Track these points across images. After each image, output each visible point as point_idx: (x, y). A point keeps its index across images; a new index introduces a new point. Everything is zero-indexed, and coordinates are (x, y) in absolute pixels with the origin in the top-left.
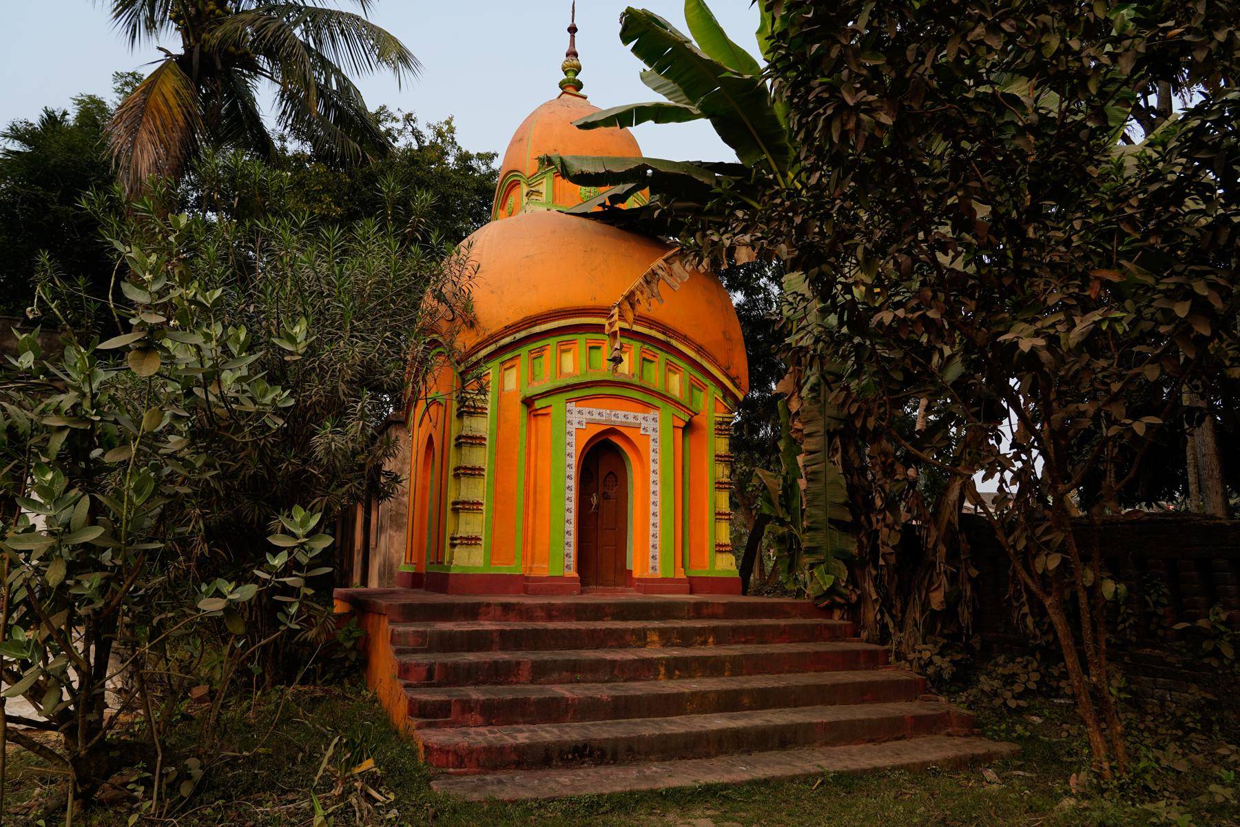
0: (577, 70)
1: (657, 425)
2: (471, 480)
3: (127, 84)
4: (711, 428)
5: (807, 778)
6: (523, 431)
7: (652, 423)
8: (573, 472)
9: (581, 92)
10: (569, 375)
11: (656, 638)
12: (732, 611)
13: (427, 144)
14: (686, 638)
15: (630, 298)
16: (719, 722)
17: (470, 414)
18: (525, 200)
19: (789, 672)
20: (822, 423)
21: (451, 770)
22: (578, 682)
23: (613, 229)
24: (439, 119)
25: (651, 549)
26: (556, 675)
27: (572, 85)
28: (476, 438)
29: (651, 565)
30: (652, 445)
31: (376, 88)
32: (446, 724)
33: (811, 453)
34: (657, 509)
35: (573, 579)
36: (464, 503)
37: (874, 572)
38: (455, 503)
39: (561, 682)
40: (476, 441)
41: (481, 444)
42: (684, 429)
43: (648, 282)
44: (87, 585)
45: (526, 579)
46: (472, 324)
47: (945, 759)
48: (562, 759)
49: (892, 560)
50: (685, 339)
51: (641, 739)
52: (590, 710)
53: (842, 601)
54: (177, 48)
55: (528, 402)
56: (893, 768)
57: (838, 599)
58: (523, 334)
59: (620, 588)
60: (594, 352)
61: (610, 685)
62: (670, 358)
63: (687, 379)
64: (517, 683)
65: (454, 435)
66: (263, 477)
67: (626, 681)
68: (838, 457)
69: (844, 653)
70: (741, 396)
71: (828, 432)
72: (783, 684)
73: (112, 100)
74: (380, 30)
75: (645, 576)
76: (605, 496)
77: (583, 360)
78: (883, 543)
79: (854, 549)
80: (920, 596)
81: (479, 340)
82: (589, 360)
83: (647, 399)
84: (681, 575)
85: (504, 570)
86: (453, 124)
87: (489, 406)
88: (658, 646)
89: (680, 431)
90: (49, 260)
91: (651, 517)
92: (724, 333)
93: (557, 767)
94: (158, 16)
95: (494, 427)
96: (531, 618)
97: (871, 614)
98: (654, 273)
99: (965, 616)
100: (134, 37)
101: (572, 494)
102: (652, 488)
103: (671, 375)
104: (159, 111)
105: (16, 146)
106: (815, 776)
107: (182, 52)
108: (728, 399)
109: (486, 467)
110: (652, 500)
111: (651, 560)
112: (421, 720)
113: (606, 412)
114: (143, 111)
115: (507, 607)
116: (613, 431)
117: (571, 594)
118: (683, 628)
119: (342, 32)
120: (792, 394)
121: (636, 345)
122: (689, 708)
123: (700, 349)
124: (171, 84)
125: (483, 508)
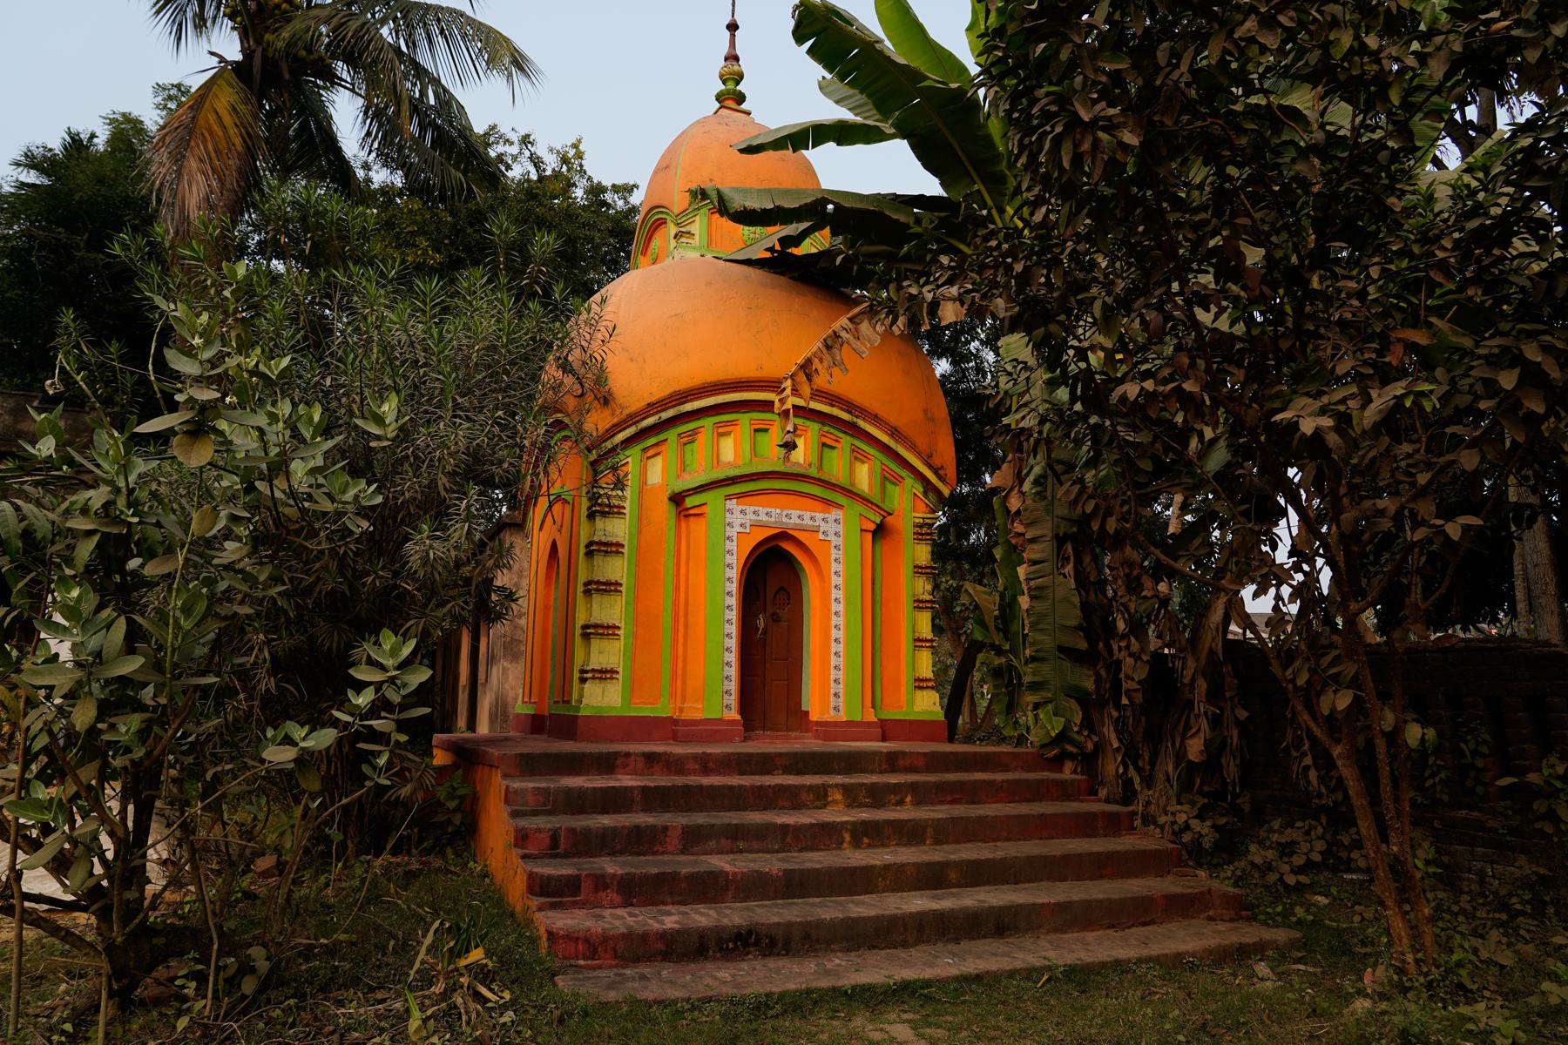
0: (739, 78)
1: (840, 528)
2: (606, 598)
3: (170, 98)
4: (908, 530)
5: (1030, 974)
8: (733, 587)
9: (744, 106)
11: (839, 797)
12: (935, 762)
14: (878, 795)
15: (806, 367)
16: (919, 903)
17: (604, 514)
18: (673, 243)
20: (1049, 524)
21: (581, 962)
22: (741, 852)
23: (782, 280)
24: (563, 141)
25: (833, 685)
26: (712, 844)
27: (732, 98)
28: (612, 544)
29: (832, 705)
30: (834, 554)
31: (484, 102)
32: (575, 905)
33: (1035, 563)
34: (840, 634)
35: (733, 722)
36: (596, 626)
37: (1115, 714)
38: (585, 627)
39: (720, 852)
40: (611, 548)
41: (618, 552)
42: (874, 533)
43: (828, 348)
44: (123, 729)
46: (606, 400)
47: (1205, 950)
48: (721, 949)
50: (875, 419)
51: (820, 923)
53: (1074, 750)
55: (677, 499)
56: (1139, 961)
57: (1070, 748)
58: (670, 413)
59: (793, 734)
60: (760, 436)
64: (663, 853)
65: (583, 541)
67: (800, 851)
69: (1077, 816)
70: (946, 492)
71: (1057, 536)
72: (999, 854)
73: (152, 119)
75: (826, 718)
76: (775, 618)
77: (746, 447)
79: (1089, 685)
81: (615, 420)
84: (871, 718)
85: (647, 711)
86: (582, 148)
87: (627, 504)
88: (841, 807)
89: (870, 536)
90: (74, 320)
91: (833, 644)
92: (925, 411)
93: (715, 959)
95: (635, 531)
96: (681, 772)
97: (1111, 767)
98: (836, 335)
99: (1231, 768)
100: (179, 39)
101: (733, 615)
102: (834, 607)
103: (858, 464)
104: (211, 132)
105: (31, 177)
106: (1041, 970)
108: (931, 495)
109: (624, 581)
110: (833, 623)
111: (832, 699)
112: (542, 900)
113: (775, 511)
114: (191, 132)
115: (651, 758)
116: (784, 535)
117: (732, 741)
118: (873, 784)
119: (442, 32)
120: (1012, 489)
121: (814, 427)
122: (881, 884)
123: (894, 432)
124: (225, 99)
125: (621, 632)
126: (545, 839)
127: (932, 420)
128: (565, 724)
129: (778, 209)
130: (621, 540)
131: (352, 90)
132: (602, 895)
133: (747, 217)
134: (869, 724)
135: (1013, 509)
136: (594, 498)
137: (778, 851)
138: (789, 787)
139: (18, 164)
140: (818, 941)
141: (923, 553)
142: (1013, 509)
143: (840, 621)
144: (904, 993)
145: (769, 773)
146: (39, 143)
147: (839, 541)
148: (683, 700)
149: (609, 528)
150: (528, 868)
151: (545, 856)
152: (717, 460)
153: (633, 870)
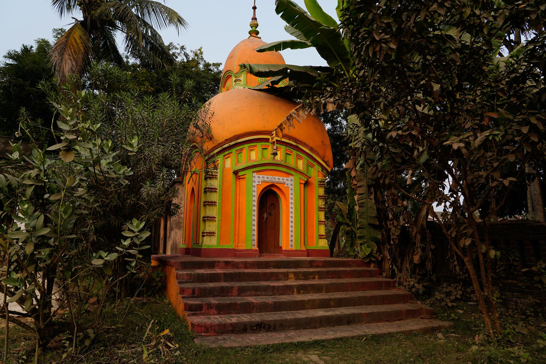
0: (257, 26)
1: (292, 183)
2: (211, 207)
3: (58, 34)
4: (316, 183)
5: (359, 337)
6: (234, 185)
7: (290, 181)
9: (259, 36)
10: (254, 161)
11: (292, 276)
12: (326, 264)
14: (306, 276)
15: (280, 127)
16: (320, 313)
17: (210, 178)
18: (234, 83)
19: (351, 291)
20: (365, 181)
21: (203, 334)
22: (258, 295)
24: (196, 48)
25: (290, 237)
26: (249, 293)
27: (254, 33)
28: (213, 189)
29: (290, 244)
30: (290, 192)
31: (168, 35)
32: (201, 314)
33: (360, 194)
34: (293, 220)
36: (208, 217)
37: (389, 247)
38: (204, 217)
39: (251, 295)
40: (213, 190)
41: (215, 191)
42: (304, 184)
43: (288, 120)
44: (43, 254)
45: (236, 250)
46: (211, 138)
48: (252, 329)
50: (305, 145)
51: (286, 320)
52: (264, 308)
53: (374, 260)
55: (236, 173)
56: (397, 333)
57: (373, 259)
58: (233, 143)
60: (264, 151)
62: (298, 153)
63: (306, 162)
64: (231, 296)
65: (203, 188)
66: (120, 206)
67: (279, 295)
68: (372, 197)
70: (329, 170)
71: (368, 185)
72: (348, 296)
73: (52, 41)
74: (170, 9)
75: (288, 249)
76: (270, 214)
77: (260, 154)
78: (393, 234)
79: (380, 237)
80: (409, 257)
81: (214, 145)
82: (262, 154)
83: (288, 171)
84: (303, 248)
85: (226, 247)
88: (293, 280)
89: (303, 185)
90: (25, 111)
92: (322, 142)
93: (250, 333)
95: (221, 184)
96: (237, 268)
97: (387, 265)
98: (291, 115)
100: (62, 13)
101: (255, 213)
102: (291, 210)
103: (299, 160)
104: (73, 46)
105: (10, 61)
106: (363, 336)
107: (82, 19)
109: (217, 201)
113: (270, 177)
114: (66, 45)
115: (227, 263)
116: (273, 185)
117: (255, 257)
120: (352, 169)
121: (283, 148)
122: (307, 307)
123: (311, 149)
124: (78, 34)
125: (216, 219)
127: (324, 145)
130: (216, 187)
132: (210, 310)
133: (260, 74)
136: (207, 173)
137: (271, 295)
138: (275, 273)
139: (6, 57)
140: (285, 327)
141: (322, 191)
144: (316, 344)
147: (292, 187)
148: (238, 243)
149: (212, 183)
150: (185, 301)
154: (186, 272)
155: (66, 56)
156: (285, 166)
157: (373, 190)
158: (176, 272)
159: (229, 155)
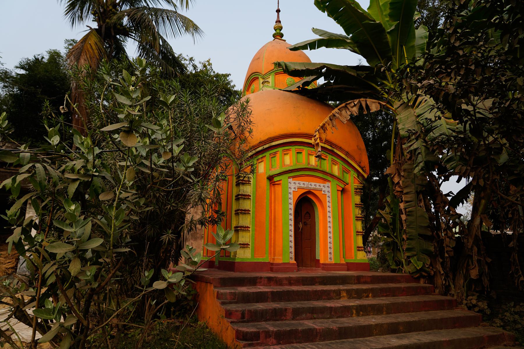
0: (281, 28)
1: (329, 189)
2: (244, 216)
3: (71, 45)
4: (352, 191)
6: (268, 192)
8: (292, 212)
9: (283, 38)
10: (288, 165)
11: (345, 294)
13: (199, 70)
15: (323, 127)
18: (261, 85)
20: (413, 187)
22: (315, 319)
23: (305, 98)
24: (204, 60)
25: (329, 249)
26: (304, 315)
27: (278, 35)
28: (246, 195)
29: (329, 257)
31: (180, 44)
32: (258, 344)
33: (407, 202)
35: (293, 264)
36: (241, 227)
37: (441, 260)
40: (246, 197)
41: (248, 199)
43: (331, 120)
44: (89, 274)
49: (452, 254)
50: (340, 149)
53: (426, 274)
54: (95, 25)
55: (270, 178)
57: (424, 274)
59: (314, 268)
60: (299, 155)
61: (331, 320)
62: (334, 158)
64: (286, 320)
67: (337, 318)
68: (422, 204)
70: (366, 176)
71: (417, 192)
72: (416, 319)
73: (63, 52)
74: (185, 18)
75: (327, 262)
78: (447, 246)
80: (463, 272)
82: (297, 158)
84: (343, 262)
85: (261, 260)
86: (210, 62)
88: (346, 298)
89: (340, 192)
90: (49, 104)
91: (329, 234)
92: (357, 146)
94: (84, 15)
95: (255, 190)
96: (281, 285)
97: (440, 281)
98: (334, 116)
99: (486, 282)
100: (73, 23)
101: (292, 223)
102: (328, 219)
103: (334, 166)
105: (22, 72)
107: (97, 27)
108: (360, 178)
109: (251, 210)
110: (328, 226)
112: (245, 342)
114: (82, 50)
115: (270, 279)
116: (309, 192)
117: (293, 271)
118: (357, 289)
119: (168, 18)
120: (395, 174)
123: (347, 154)
124: (93, 40)
125: (250, 229)
126: (239, 314)
127: (360, 149)
128: (230, 265)
129: (308, 69)
131: (135, 39)
133: (295, 73)
134: (342, 264)
135: (396, 182)
136: (238, 177)
137: (328, 318)
138: (326, 291)
139: (17, 67)
141: (357, 199)
142: (396, 182)
143: (331, 225)
145: (314, 285)
146: (26, 57)
147: (329, 194)
148: (274, 255)
149: (245, 189)
150: (236, 327)
151: (240, 322)
152: (284, 165)
153: (279, 329)
154: (228, 291)
155: (82, 61)
156: (322, 171)
157: (422, 197)
158: (216, 290)
159: (263, 159)
